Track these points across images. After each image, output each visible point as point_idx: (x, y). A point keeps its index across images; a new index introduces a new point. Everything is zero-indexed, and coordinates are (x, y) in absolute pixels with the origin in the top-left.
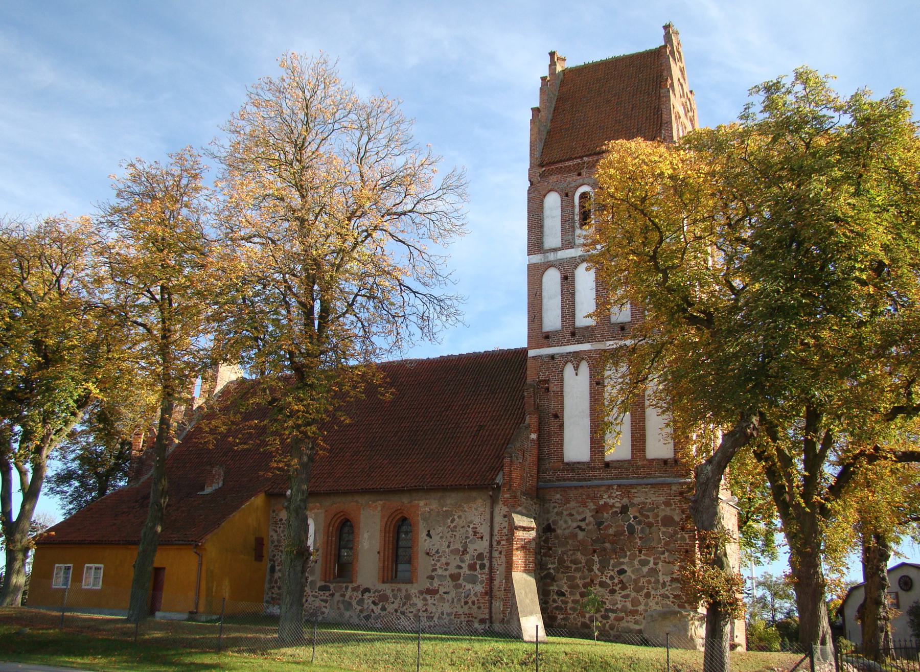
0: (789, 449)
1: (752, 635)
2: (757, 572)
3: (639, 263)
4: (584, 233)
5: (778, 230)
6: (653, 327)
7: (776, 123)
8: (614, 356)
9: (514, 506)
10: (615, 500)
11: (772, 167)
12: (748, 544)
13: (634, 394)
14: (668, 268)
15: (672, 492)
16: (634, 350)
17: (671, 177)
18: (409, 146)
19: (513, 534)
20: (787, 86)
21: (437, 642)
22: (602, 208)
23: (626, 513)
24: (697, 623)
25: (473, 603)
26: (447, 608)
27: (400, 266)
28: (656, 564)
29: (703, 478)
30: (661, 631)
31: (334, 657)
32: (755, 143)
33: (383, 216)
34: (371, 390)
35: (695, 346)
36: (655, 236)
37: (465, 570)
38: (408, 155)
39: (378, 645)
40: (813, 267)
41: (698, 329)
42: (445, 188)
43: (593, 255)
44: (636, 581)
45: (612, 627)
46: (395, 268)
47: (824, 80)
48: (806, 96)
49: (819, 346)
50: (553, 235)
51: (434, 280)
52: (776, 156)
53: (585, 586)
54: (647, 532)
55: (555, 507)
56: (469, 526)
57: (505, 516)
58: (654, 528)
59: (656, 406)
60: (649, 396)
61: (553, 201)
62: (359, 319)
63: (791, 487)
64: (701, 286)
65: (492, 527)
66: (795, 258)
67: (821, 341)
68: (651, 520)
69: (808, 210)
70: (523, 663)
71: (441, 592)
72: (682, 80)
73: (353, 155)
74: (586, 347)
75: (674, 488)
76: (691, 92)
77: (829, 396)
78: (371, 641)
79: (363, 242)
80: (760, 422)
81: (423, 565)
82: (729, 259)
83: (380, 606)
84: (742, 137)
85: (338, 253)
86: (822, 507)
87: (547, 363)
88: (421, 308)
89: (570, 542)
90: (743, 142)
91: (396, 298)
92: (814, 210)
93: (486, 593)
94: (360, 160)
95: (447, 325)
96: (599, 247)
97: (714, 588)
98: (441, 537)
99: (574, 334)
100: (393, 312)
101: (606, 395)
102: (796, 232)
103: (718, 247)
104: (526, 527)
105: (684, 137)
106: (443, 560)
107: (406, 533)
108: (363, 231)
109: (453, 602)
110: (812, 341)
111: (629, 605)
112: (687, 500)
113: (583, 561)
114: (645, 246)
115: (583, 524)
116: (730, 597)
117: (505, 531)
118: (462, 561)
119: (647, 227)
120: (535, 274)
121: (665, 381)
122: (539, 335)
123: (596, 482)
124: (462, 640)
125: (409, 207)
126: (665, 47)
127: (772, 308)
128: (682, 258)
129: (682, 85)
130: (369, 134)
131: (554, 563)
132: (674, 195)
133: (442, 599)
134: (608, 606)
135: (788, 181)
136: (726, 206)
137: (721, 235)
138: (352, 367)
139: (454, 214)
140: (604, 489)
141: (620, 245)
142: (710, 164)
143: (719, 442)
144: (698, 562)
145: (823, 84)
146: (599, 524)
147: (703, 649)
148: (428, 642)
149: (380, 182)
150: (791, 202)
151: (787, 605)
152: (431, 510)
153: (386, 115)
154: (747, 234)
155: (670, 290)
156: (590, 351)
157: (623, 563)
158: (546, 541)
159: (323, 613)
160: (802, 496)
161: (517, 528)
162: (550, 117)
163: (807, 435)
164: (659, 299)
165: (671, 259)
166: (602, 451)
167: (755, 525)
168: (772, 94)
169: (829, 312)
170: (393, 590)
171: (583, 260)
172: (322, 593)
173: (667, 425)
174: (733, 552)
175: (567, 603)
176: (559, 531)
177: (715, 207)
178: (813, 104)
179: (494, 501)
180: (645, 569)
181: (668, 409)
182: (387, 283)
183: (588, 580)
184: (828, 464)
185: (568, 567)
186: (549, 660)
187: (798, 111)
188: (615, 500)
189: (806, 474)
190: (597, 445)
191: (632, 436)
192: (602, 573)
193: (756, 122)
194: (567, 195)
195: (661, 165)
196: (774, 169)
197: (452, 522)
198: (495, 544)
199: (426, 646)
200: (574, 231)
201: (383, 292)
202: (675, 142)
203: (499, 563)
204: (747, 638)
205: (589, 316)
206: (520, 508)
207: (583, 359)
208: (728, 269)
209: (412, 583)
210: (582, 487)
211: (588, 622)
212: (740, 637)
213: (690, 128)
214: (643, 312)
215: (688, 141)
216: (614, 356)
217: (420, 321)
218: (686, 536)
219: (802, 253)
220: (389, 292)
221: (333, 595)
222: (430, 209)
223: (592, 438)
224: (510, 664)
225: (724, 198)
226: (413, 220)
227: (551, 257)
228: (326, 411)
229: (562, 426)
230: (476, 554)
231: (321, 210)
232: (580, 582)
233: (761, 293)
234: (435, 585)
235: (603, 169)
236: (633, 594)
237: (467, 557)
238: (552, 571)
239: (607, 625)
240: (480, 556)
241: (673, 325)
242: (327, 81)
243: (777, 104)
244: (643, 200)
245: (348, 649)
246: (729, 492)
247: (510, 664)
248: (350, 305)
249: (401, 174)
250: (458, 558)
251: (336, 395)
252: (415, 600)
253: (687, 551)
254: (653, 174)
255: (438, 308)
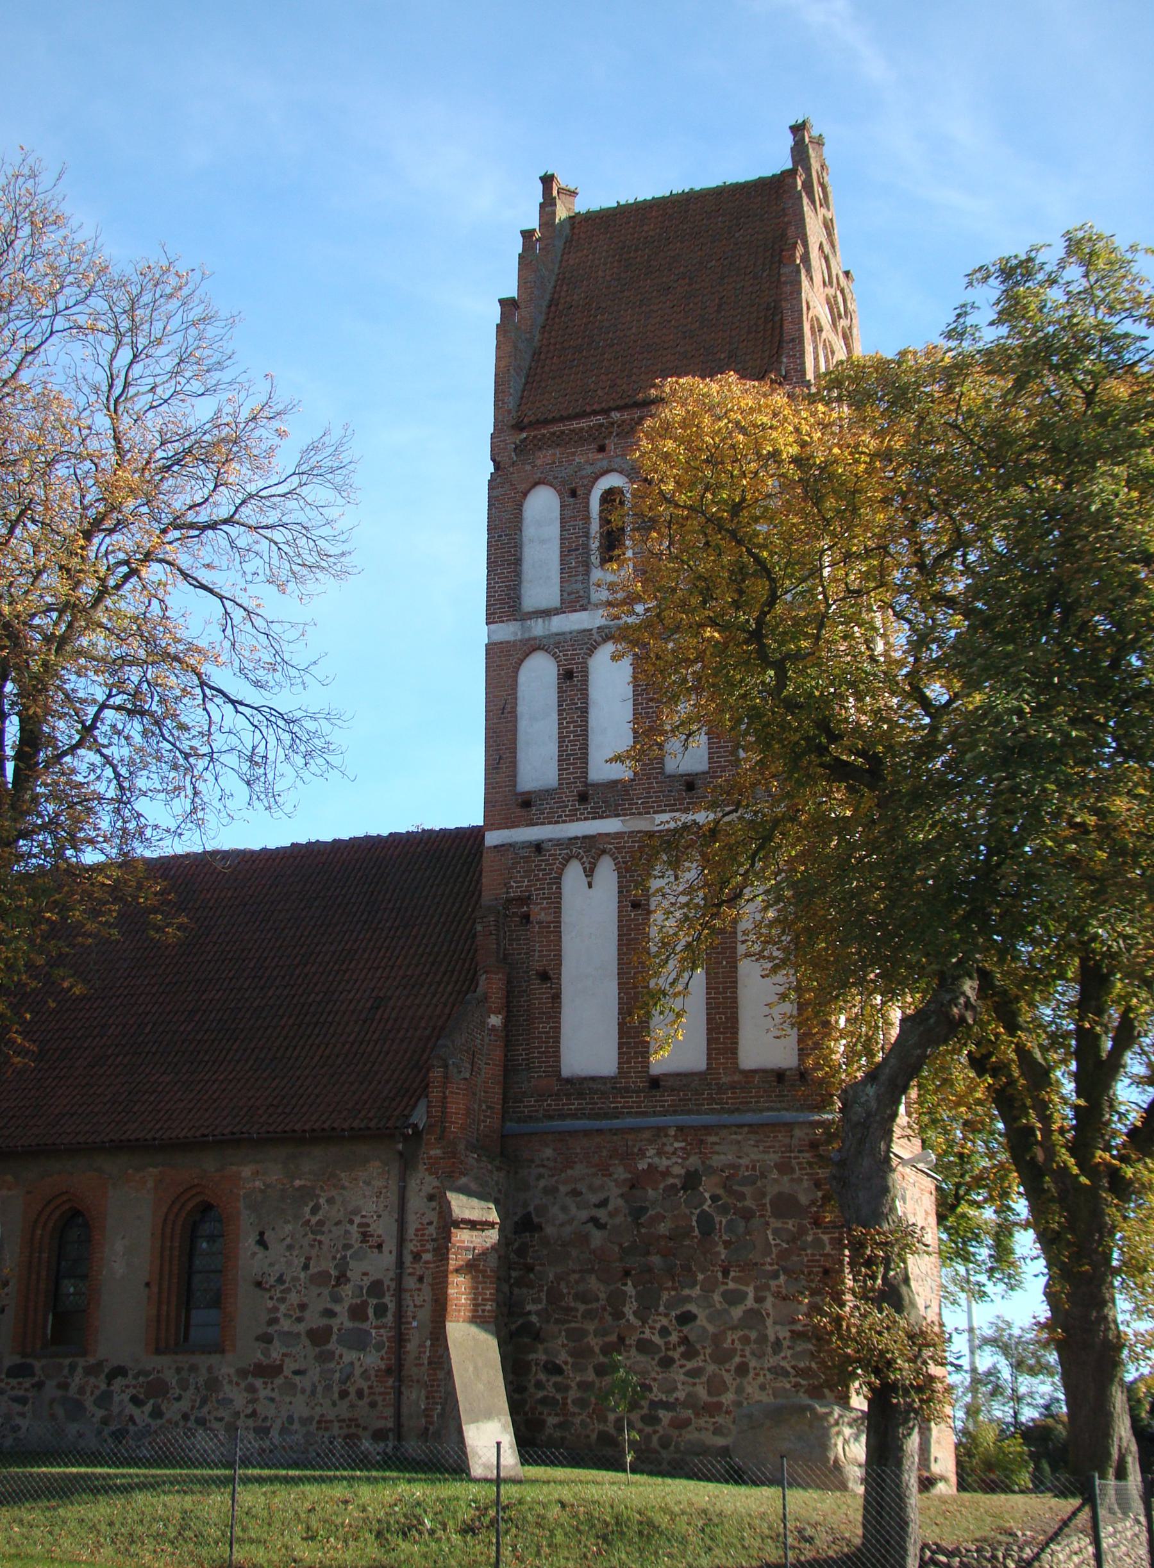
0: (1044, 1049)
1: (970, 1454)
2: (984, 1316)
3: (726, 645)
4: (611, 578)
5: (1021, 579)
6: (753, 785)
7: (1025, 348)
8: (671, 846)
9: (451, 1176)
10: (672, 1161)
11: (1011, 443)
12: (958, 1255)
13: (712, 928)
14: (788, 656)
15: (795, 1142)
16: (713, 833)
17: (796, 460)
18: (226, 376)
19: (448, 1238)
20: (1048, 268)
21: (277, 1486)
22: (647, 524)
23: (694, 1188)
24: (847, 1431)
25: (360, 1394)
26: (299, 1407)
27: (202, 643)
28: (759, 1300)
29: (858, 1112)
30: (776, 1451)
31: (37, 1533)
32: (979, 389)
33: (164, 531)
34: (134, 919)
35: (843, 826)
36: (761, 588)
37: (342, 1320)
38: (222, 396)
39: (141, 1498)
40: (1096, 661)
41: (851, 789)
42: (306, 473)
43: (627, 627)
44: (717, 1339)
45: (665, 1443)
46: (192, 648)
47: (1129, 256)
48: (1088, 291)
49: (1108, 829)
50: (542, 583)
51: (278, 675)
52: (1021, 421)
53: (607, 1350)
54: (741, 1230)
55: (540, 1177)
56: (351, 1222)
57: (431, 1198)
58: (756, 1222)
59: (760, 956)
60: (745, 933)
61: (542, 507)
62: (108, 760)
63: (1047, 1132)
64: (859, 698)
65: (402, 1223)
66: (1057, 639)
67: (1110, 820)
68: (749, 1203)
69: (1085, 537)
70: (468, 1530)
71: (287, 1372)
72: (827, 248)
73: (96, 390)
74: (611, 825)
75: (798, 1133)
76: (847, 274)
77: (1126, 937)
78: (126, 1489)
79: (118, 587)
80: (981, 992)
81: (247, 1309)
82: (920, 642)
83: (148, 1408)
84: (949, 376)
85: (61, 612)
86: (1114, 1174)
87: (527, 859)
88: (249, 738)
89: (574, 1253)
90: (950, 389)
91: (192, 714)
92: (1098, 539)
93: (389, 1371)
94: (114, 407)
95: (306, 775)
96: (639, 608)
97: (882, 1353)
98: (290, 1247)
99: (588, 797)
100: (185, 746)
101: (654, 932)
102: (1061, 585)
103: (896, 614)
104: (476, 1221)
105: (826, 374)
106: (294, 1298)
107: (212, 1239)
108: (120, 563)
109: (313, 1393)
110: (1092, 820)
111: (702, 1392)
112: (823, 1160)
113: (602, 1296)
114: (738, 608)
115: (602, 1214)
116: (918, 1372)
117: (432, 1230)
118: (337, 1299)
119: (743, 568)
120: (503, 665)
121: (777, 902)
122: (506, 796)
123: (630, 1122)
124: (331, 1480)
125: (224, 512)
126: (792, 173)
127: (1006, 748)
128: (817, 638)
129: (827, 259)
130: (134, 345)
131: (539, 1301)
132: (804, 500)
133: (290, 1387)
134: (657, 1395)
135: (1048, 473)
136: (914, 524)
137: (901, 589)
138: (92, 868)
139: (326, 531)
140: (646, 1135)
141: (684, 606)
142: (879, 434)
143: (895, 1032)
144: (848, 1297)
145: (1124, 263)
146: (637, 1213)
147: (861, 1490)
148: (255, 1487)
149: (160, 454)
150: (1051, 518)
151: (1046, 1388)
152: (267, 1186)
153: (174, 304)
154: (957, 586)
155: (791, 705)
156: (619, 835)
157: (688, 1299)
158: (521, 1252)
159: (16, 1429)
160: (1072, 1151)
161: (457, 1224)
162: (541, 319)
163: (1082, 1019)
164: (768, 724)
165: (795, 639)
166: (643, 1051)
167: (972, 1212)
168: (1017, 284)
169: (1127, 756)
170: (178, 1370)
171: (606, 635)
172: (13, 1382)
173: (783, 997)
174: (925, 1275)
175: (567, 1388)
176: (549, 1230)
177: (889, 529)
178: (1103, 309)
179: (407, 1163)
180: (737, 1312)
181: (784, 962)
182: (175, 680)
183: (613, 1338)
184: (1127, 1081)
185: (568, 1310)
186: (525, 1518)
187: (1069, 325)
188: (672, 1161)
189: (1081, 1102)
190: (633, 1038)
191: (709, 1020)
192: (644, 1322)
193: (980, 345)
194: (573, 493)
195: (775, 434)
196: (1016, 449)
197: (315, 1210)
198: (408, 1259)
199: (251, 1497)
200: (587, 573)
201: (163, 701)
202: (808, 385)
203: (418, 1299)
204: (959, 1464)
205: (618, 758)
206: (463, 1180)
207: (604, 852)
208: (917, 660)
209: (223, 1352)
210: (600, 1131)
211: (612, 1431)
212: (944, 1461)
213: (841, 355)
214: (734, 752)
215: (837, 383)
216: (671, 846)
217: (245, 766)
218: (825, 1238)
219: (1073, 629)
220: (178, 699)
221: (39, 1386)
222: (272, 517)
223: (621, 1025)
224: (440, 1533)
225: (913, 504)
226: (232, 542)
227: (538, 628)
228: (30, 966)
229: (557, 997)
230: (367, 1282)
231: (23, 513)
232: (595, 1342)
233: (985, 715)
234: (274, 1355)
235: (652, 440)
236: (711, 1368)
237: (347, 1290)
238: (534, 1319)
239: (655, 1438)
240: (376, 1288)
241: (797, 780)
242: (38, 219)
243: (1025, 307)
244: (736, 509)
245: (71, 1512)
246: (917, 1142)
247: (440, 1533)
248: (88, 730)
249: (207, 437)
250: (326, 1292)
251: (54, 931)
252: (229, 1391)
253: (826, 1272)
254: (759, 456)
255: (286, 737)
